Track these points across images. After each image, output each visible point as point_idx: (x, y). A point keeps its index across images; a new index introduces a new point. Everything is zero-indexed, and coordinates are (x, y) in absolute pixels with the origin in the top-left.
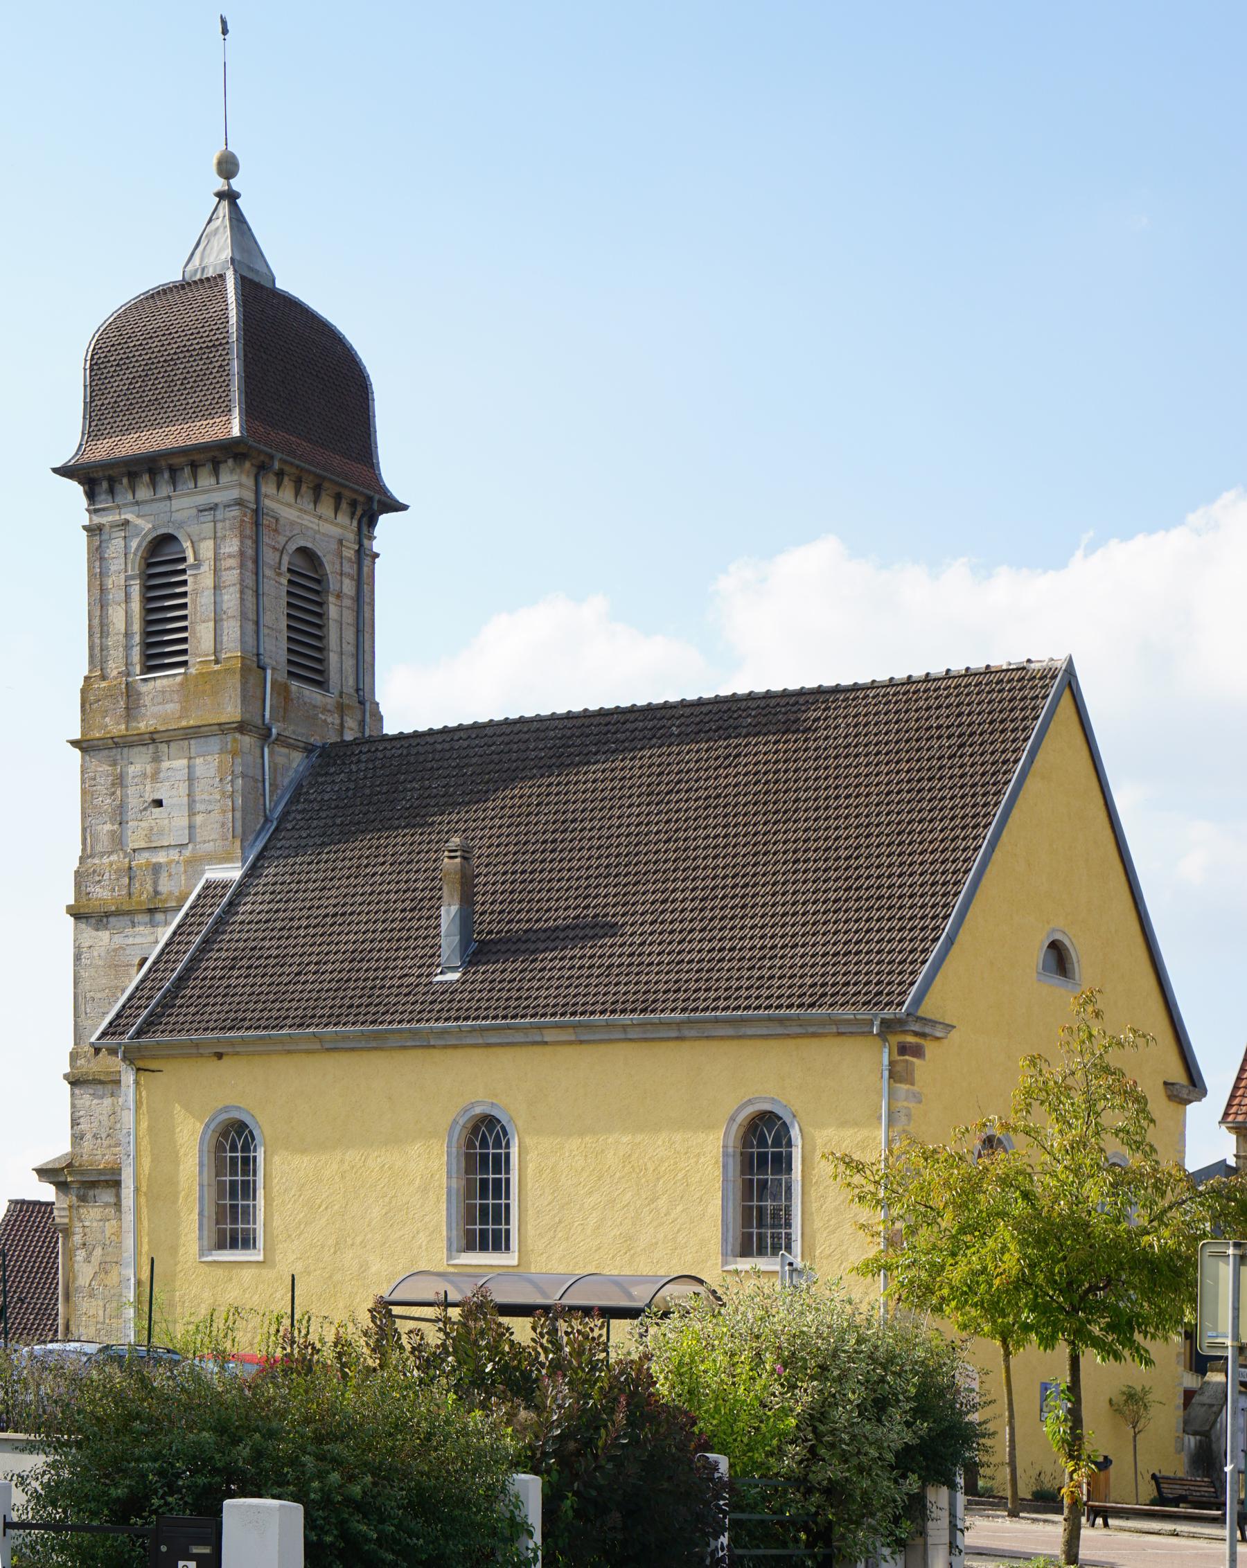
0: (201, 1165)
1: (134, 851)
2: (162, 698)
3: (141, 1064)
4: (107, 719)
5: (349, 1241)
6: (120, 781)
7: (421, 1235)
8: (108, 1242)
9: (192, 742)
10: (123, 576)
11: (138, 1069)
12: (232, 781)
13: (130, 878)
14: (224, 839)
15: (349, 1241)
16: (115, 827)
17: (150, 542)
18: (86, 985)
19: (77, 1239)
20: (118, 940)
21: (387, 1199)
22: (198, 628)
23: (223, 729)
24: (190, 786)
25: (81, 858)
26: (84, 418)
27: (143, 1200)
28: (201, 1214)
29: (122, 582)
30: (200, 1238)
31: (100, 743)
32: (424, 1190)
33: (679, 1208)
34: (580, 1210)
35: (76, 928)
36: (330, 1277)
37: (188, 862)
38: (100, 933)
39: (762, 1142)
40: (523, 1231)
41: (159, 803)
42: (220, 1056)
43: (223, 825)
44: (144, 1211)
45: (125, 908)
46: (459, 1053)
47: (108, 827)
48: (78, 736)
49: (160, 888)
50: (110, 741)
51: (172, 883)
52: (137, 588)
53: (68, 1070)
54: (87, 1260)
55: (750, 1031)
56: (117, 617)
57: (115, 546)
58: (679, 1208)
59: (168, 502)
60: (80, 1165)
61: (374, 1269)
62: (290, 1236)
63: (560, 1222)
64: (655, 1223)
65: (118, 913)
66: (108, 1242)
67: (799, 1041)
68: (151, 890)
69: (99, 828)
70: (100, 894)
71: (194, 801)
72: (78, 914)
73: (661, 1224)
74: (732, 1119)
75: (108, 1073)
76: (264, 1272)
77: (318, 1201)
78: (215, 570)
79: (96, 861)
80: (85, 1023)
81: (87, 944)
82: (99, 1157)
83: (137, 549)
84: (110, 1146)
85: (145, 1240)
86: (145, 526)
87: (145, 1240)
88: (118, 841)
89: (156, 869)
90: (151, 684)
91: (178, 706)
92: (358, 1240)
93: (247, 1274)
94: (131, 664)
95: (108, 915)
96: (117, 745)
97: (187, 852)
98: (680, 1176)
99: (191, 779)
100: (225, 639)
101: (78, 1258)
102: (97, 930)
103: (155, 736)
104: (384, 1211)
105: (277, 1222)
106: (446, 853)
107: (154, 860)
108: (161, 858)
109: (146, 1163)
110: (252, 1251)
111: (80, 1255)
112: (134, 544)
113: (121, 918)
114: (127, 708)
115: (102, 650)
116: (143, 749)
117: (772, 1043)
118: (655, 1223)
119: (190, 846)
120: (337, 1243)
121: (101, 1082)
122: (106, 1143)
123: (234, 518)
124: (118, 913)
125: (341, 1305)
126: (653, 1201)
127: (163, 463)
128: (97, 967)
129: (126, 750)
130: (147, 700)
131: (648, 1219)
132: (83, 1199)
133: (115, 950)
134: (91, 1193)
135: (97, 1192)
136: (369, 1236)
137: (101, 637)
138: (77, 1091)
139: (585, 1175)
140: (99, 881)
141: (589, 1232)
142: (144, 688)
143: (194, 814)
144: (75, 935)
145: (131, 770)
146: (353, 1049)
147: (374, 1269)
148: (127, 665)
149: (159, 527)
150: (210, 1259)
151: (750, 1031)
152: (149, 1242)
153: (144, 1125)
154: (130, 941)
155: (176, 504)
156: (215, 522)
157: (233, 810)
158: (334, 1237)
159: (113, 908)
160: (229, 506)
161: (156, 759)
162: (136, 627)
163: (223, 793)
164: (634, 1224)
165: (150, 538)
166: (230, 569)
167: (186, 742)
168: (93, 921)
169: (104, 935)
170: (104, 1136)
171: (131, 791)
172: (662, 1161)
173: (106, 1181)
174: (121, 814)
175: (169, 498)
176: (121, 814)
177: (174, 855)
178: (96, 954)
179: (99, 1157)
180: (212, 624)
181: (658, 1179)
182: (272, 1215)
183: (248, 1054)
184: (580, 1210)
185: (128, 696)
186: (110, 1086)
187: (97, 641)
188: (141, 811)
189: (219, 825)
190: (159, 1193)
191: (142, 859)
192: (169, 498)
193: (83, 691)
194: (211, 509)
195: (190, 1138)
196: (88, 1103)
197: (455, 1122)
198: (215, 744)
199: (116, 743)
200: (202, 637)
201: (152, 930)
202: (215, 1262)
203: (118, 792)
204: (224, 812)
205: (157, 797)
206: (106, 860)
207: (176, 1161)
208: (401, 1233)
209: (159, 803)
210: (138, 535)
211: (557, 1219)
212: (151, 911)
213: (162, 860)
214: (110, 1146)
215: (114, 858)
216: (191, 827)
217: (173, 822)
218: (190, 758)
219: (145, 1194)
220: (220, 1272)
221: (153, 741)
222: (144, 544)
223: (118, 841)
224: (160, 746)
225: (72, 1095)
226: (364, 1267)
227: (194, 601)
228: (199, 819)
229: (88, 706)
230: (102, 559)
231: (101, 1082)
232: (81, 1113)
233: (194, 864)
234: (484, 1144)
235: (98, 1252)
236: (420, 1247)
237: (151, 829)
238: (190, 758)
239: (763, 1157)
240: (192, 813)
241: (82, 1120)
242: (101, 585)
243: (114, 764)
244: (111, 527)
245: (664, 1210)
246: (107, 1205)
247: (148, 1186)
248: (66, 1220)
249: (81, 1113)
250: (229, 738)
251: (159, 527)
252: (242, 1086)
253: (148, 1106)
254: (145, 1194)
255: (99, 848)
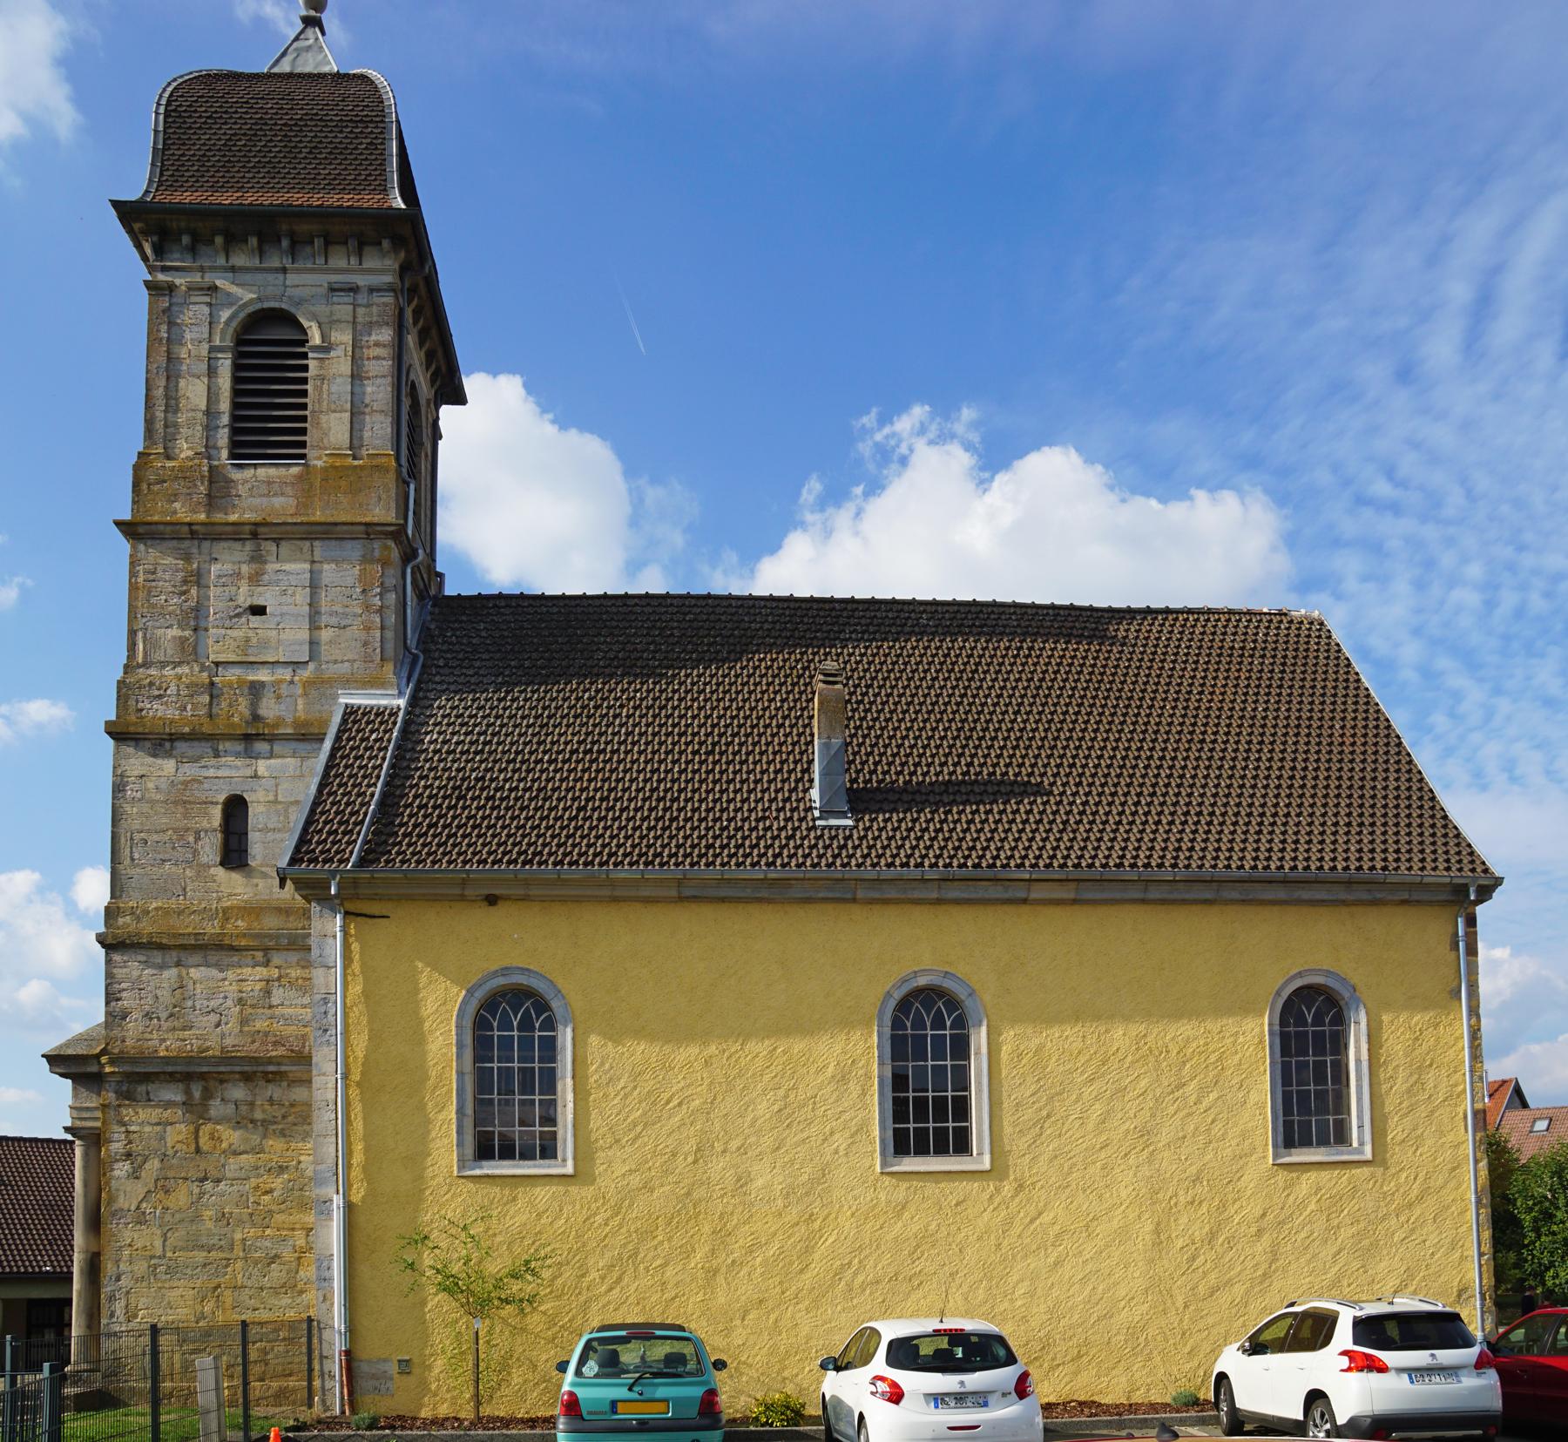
0: (460, 1045)
1: (217, 664)
2: (262, 489)
3: (350, 907)
4: (177, 505)
5: (718, 1147)
6: (197, 578)
7: (837, 1136)
8: (170, 1152)
9: (316, 543)
10: (206, 346)
11: (347, 913)
12: (381, 594)
13: (212, 696)
14: (367, 659)
15: (718, 1147)
16: (187, 633)
17: (250, 315)
18: (133, 822)
19: (117, 1147)
20: (190, 770)
21: (781, 1092)
22: (324, 418)
23: (370, 531)
24: (312, 595)
25: (126, 667)
26: (153, 164)
27: (354, 1093)
28: (460, 1111)
29: (205, 353)
30: (460, 1144)
31: (169, 529)
32: (842, 1079)
33: (1212, 1096)
34: (1077, 1101)
35: (117, 752)
36: (688, 1194)
37: (308, 684)
38: (159, 761)
39: (1301, 1020)
40: (995, 1128)
41: (259, 610)
42: (492, 900)
43: (365, 644)
44: (357, 1108)
45: (207, 729)
46: (891, 911)
47: (175, 632)
48: (127, 516)
49: (262, 712)
50: (186, 529)
51: (283, 707)
52: (228, 362)
53: (102, 929)
54: (135, 1175)
55: (1305, 895)
56: (194, 392)
57: (194, 315)
58: (1212, 1096)
59: (281, 276)
60: (121, 1052)
61: (760, 1182)
62: (617, 1141)
63: (1048, 1116)
64: (1182, 1114)
65: (194, 737)
66: (170, 1152)
67: (1354, 909)
68: (247, 713)
69: (160, 632)
70: (160, 711)
71: (318, 613)
72: (120, 733)
73: (1189, 1114)
74: (1278, 993)
75: (175, 936)
76: (573, 1189)
77: (665, 1096)
78: (353, 357)
79: (153, 672)
80: (131, 872)
81: (136, 773)
82: (156, 1043)
83: (227, 323)
84: (174, 1029)
85: (358, 1147)
86: (243, 294)
87: (358, 1147)
88: (190, 651)
89: (256, 689)
90: (249, 473)
91: (292, 502)
92: (734, 1145)
93: (543, 1193)
94: (215, 447)
95: (174, 738)
96: (193, 535)
97: (307, 673)
98: (1213, 1058)
99: (314, 586)
100: (367, 434)
101: (116, 1173)
102: (155, 756)
103: (261, 530)
104: (776, 1108)
105: (595, 1122)
106: (821, 677)
107: (251, 678)
108: (263, 676)
109: (360, 1043)
110: (552, 1162)
111: (121, 1170)
112: (225, 315)
113: (196, 744)
114: (209, 495)
115: (166, 426)
116: (238, 545)
117: (1322, 910)
118: (1182, 1114)
119: (311, 666)
120: (698, 1150)
121: (161, 947)
122: (165, 1025)
123: (386, 305)
124: (194, 737)
125: (707, 1229)
126: (1178, 1087)
127: (284, 227)
128: (152, 802)
129: (206, 544)
130: (242, 490)
131: (1171, 1110)
132: (128, 1096)
133: (186, 783)
134: (141, 1089)
135: (151, 1087)
136: (752, 1139)
137: (166, 411)
138: (117, 957)
139: (1082, 1059)
140: (160, 697)
141: (1090, 1126)
142: (236, 475)
143: (319, 628)
144: (115, 759)
145: (215, 569)
146: (723, 900)
147: (760, 1182)
148: (206, 447)
149: (267, 299)
150: (478, 1172)
151: (1305, 895)
152: (367, 1150)
153: (356, 989)
154: (211, 772)
155: (292, 279)
156: (355, 306)
157: (382, 628)
158: (693, 1141)
159: (187, 730)
160: (379, 290)
161: (257, 558)
162: (225, 405)
163: (367, 607)
164: (1153, 1116)
165: (251, 309)
166: (377, 358)
167: (308, 543)
168: (148, 744)
169: (169, 765)
170: (164, 1015)
171: (212, 592)
172: (1188, 1041)
173: (171, 1074)
174: (196, 618)
175: (284, 270)
176: (196, 618)
177: (285, 674)
178: (151, 785)
179: (156, 1043)
180: (348, 415)
181: (1184, 1063)
182: (588, 1114)
183: (542, 900)
184: (1077, 1101)
185: (211, 482)
186: (174, 954)
187: (160, 415)
188: (231, 618)
189: (359, 644)
190: (385, 1082)
191: (232, 674)
192: (284, 270)
193: (136, 468)
194: (351, 290)
195: (441, 1013)
196: (135, 973)
197: (889, 994)
198: (354, 550)
199: (192, 532)
200: (330, 429)
201: (248, 761)
202: (488, 1176)
203: (194, 591)
204: (367, 629)
205: (261, 602)
206: (168, 671)
207: (418, 1038)
208: (805, 1135)
209: (259, 610)
210: (232, 304)
211: (1044, 1113)
212: (248, 738)
213: (263, 679)
214: (174, 1029)
215: (185, 669)
216: (313, 643)
217: (285, 634)
218: (313, 562)
219: (358, 1084)
220: (495, 1191)
221: (255, 536)
222: (242, 315)
223: (190, 651)
224: (264, 544)
225: (108, 962)
226: (743, 1181)
227: (319, 389)
228: (325, 635)
229: (144, 486)
230: (171, 324)
231: (161, 947)
232: (123, 985)
233: (321, 686)
234: (919, 1024)
235: (154, 1165)
236: (836, 1152)
237: (248, 640)
238: (313, 562)
239: (1302, 1036)
240: (314, 627)
241: (124, 994)
242: (168, 352)
243: (187, 558)
244: (189, 289)
245: (1193, 1098)
246: (168, 1105)
247: (362, 1073)
248: (98, 1124)
249: (123, 985)
250: (377, 545)
251: (267, 299)
252: (523, 943)
253: (363, 964)
254: (358, 1084)
255: (159, 656)
